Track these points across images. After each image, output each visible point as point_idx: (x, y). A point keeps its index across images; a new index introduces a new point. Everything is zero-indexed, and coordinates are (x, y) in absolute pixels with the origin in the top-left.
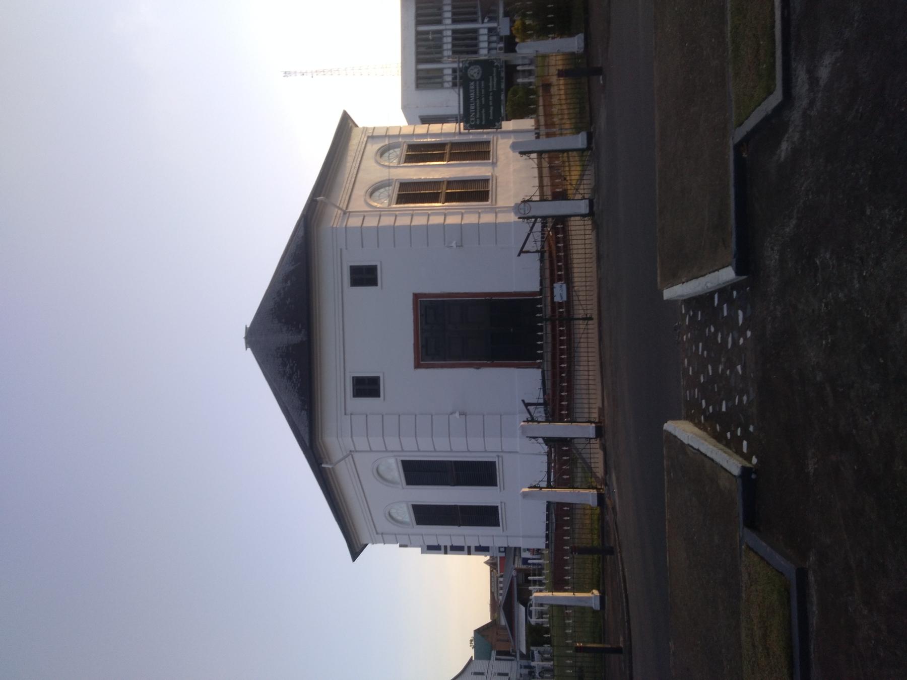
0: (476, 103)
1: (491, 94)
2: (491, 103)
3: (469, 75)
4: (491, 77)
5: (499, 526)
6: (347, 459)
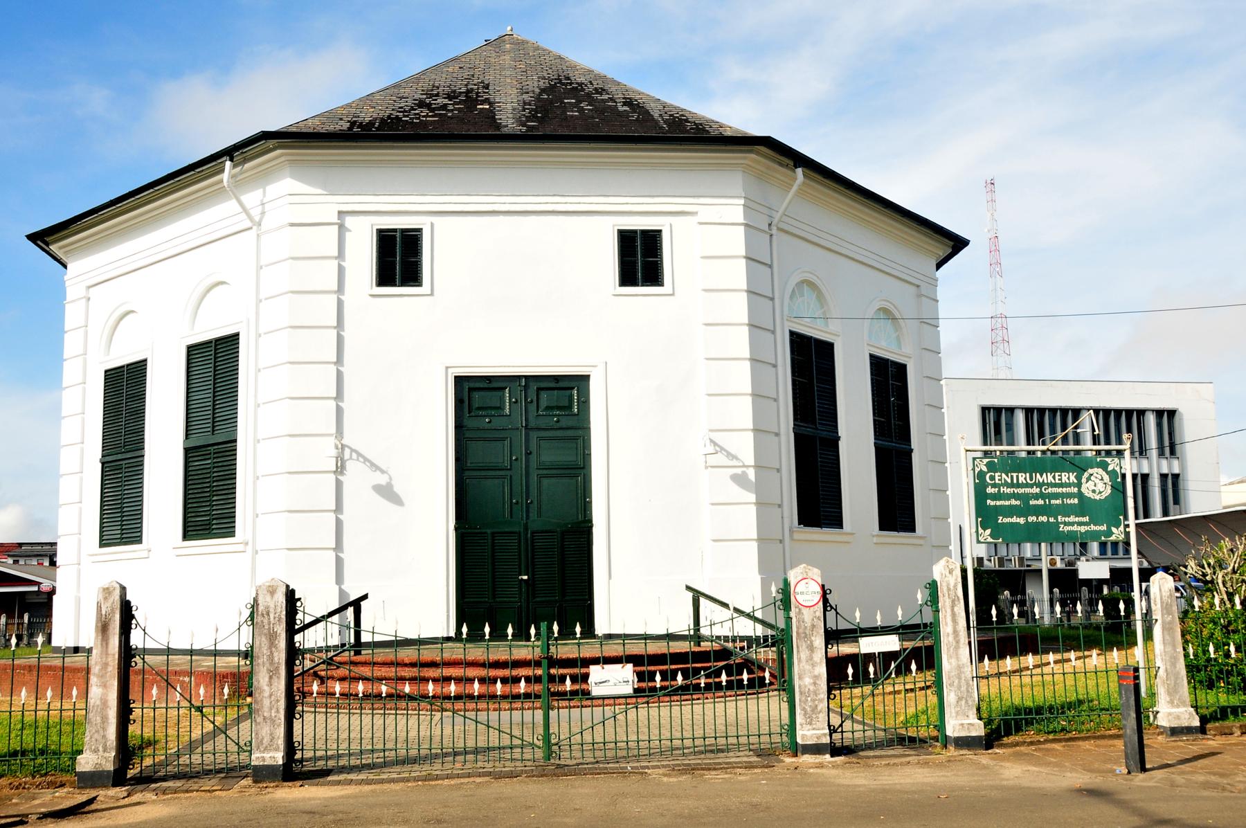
1: (1052, 520)
2: (1032, 519)
4: (1086, 519)
6: (244, 216)
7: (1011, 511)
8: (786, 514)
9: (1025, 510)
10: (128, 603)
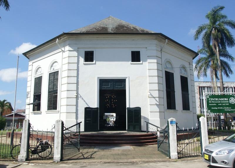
0: (218, 101)
1: (223, 108)
2: (219, 108)
3: (231, 98)
5: (48, 110)
7: (214, 106)
8: (165, 106)
9: (217, 106)
10: (30, 123)
